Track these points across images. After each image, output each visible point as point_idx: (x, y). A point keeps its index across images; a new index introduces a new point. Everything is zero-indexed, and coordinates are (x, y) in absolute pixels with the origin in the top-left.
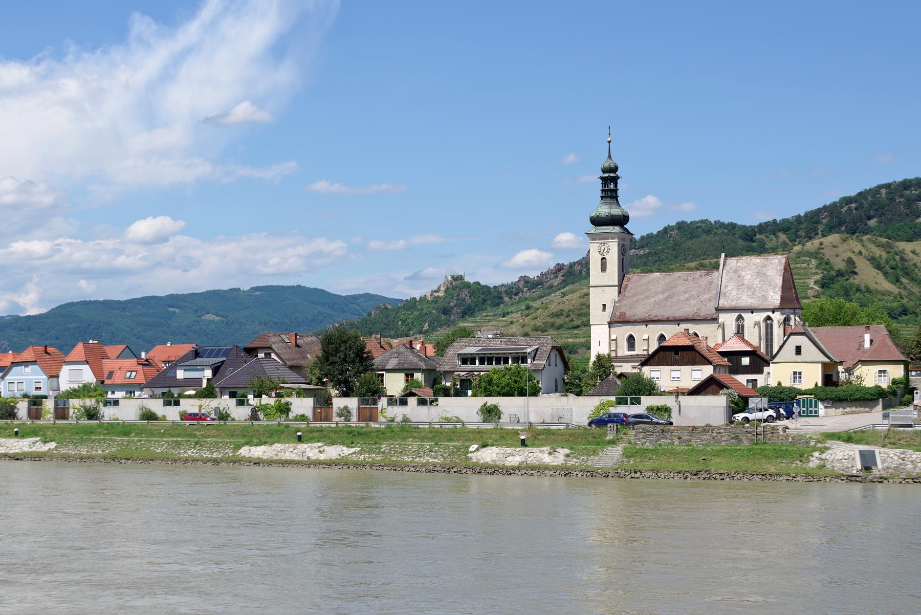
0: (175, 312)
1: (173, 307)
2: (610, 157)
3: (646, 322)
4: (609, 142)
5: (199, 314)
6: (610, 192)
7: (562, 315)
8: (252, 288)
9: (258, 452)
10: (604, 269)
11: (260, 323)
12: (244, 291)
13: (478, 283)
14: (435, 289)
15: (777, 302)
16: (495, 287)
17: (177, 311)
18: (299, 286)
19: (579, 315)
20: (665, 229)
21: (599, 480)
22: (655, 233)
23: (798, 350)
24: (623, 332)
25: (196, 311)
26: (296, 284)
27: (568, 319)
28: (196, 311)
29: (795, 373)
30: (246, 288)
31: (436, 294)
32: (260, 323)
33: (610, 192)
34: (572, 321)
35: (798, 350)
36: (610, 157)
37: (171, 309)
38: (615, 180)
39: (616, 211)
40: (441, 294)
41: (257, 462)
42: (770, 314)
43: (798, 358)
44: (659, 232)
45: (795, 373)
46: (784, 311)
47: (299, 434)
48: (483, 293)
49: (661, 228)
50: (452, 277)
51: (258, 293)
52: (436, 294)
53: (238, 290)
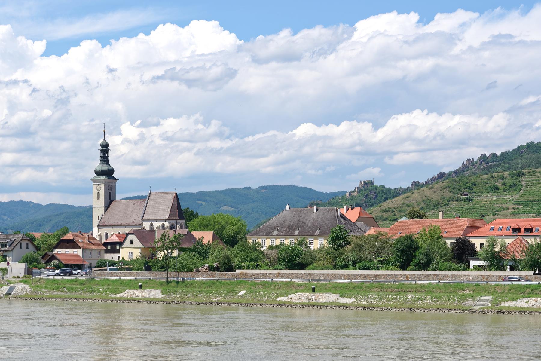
0: (202, 205)
1: (201, 200)
2: (105, 139)
3: (113, 226)
4: (104, 131)
5: (219, 206)
6: (105, 159)
7: (389, 211)
8: (260, 187)
9: (522, 303)
10: (98, 198)
11: (263, 212)
12: (253, 190)
13: (383, 187)
14: (353, 190)
15: (167, 217)
16: (395, 189)
17: (204, 203)
18: (294, 186)
19: (400, 211)
20: (519, 147)
21: (38, 301)
22: (511, 150)
23: (132, 242)
24: (104, 231)
25: (217, 204)
26: (291, 184)
27: (393, 214)
28: (217, 204)
29: (130, 253)
30: (255, 187)
31: (352, 194)
32: (263, 212)
33: (105, 159)
34: (395, 215)
35: (132, 242)
36: (105, 139)
37: (199, 202)
38: (107, 151)
39: (105, 167)
40: (356, 194)
41: (522, 311)
42: (164, 223)
43: (132, 246)
44: (514, 150)
45: (130, 253)
46: (170, 221)
47: (313, 287)
48: (386, 194)
49: (516, 147)
50: (365, 182)
51: (263, 191)
52: (352, 194)
53: (249, 188)
